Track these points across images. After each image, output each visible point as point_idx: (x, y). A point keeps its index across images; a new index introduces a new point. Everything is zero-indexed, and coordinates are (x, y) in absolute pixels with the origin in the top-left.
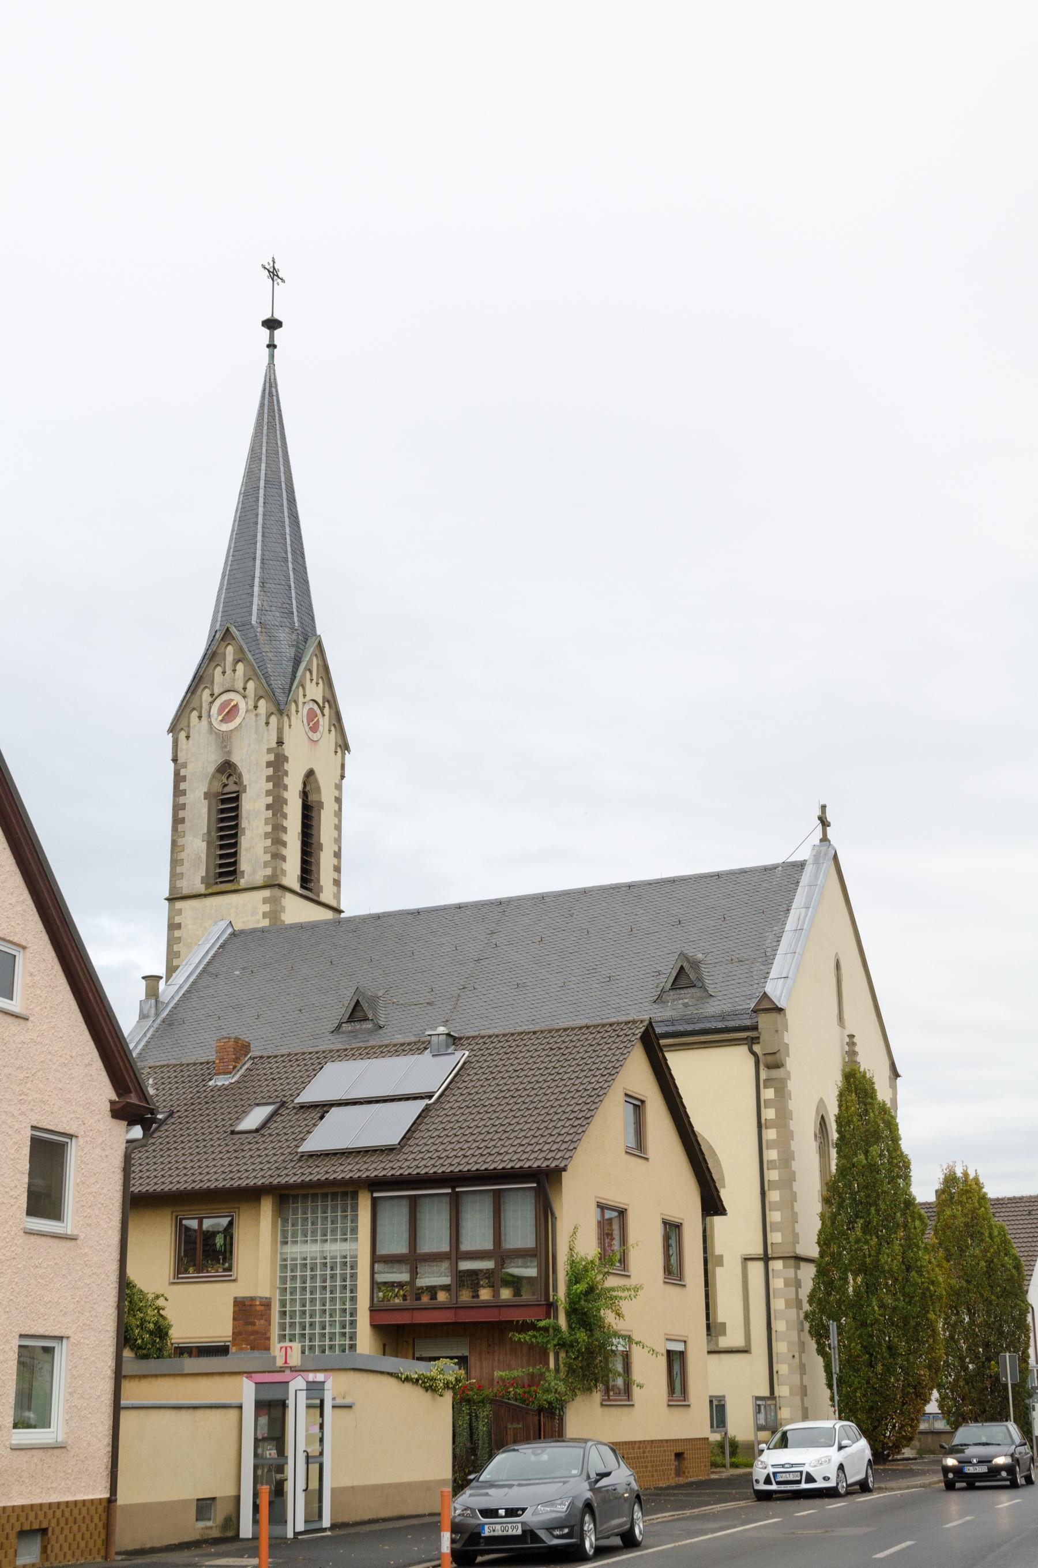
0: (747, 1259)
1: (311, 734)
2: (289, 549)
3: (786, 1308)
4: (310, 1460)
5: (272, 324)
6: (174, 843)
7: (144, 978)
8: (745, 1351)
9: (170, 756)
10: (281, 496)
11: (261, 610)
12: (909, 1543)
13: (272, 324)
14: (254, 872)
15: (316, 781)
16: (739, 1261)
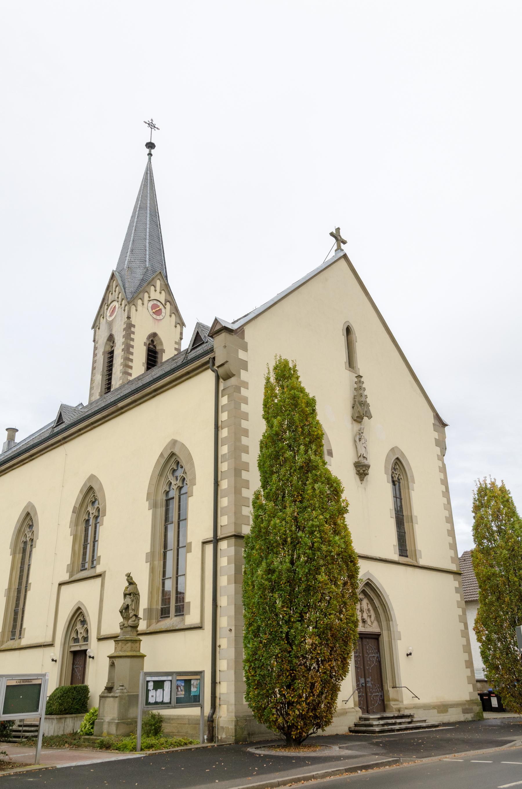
0: (204, 543)
1: (155, 316)
2: (148, 234)
3: (228, 584)
4: (395, 686)
5: (150, 146)
6: (92, 379)
7: (7, 430)
8: (200, 628)
9: (92, 339)
10: (146, 213)
11: (130, 262)
12: (501, 787)
13: (150, 146)
14: (116, 383)
15: (160, 339)
16: (201, 544)
